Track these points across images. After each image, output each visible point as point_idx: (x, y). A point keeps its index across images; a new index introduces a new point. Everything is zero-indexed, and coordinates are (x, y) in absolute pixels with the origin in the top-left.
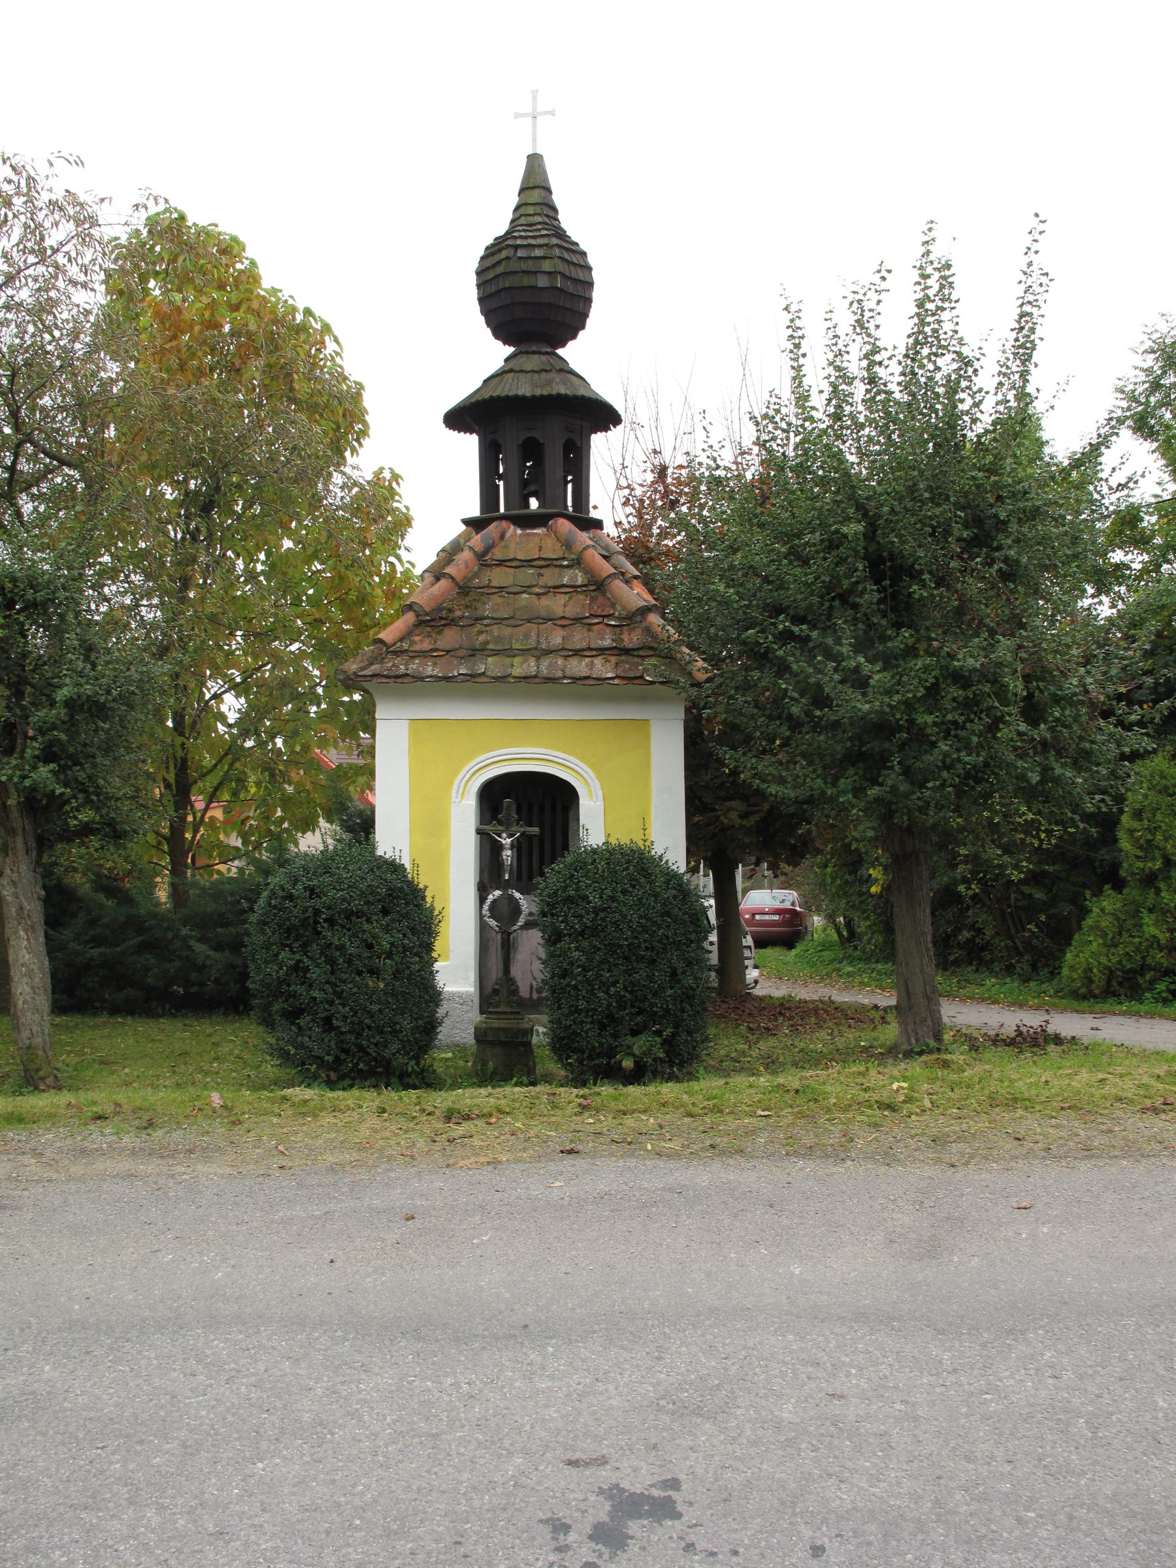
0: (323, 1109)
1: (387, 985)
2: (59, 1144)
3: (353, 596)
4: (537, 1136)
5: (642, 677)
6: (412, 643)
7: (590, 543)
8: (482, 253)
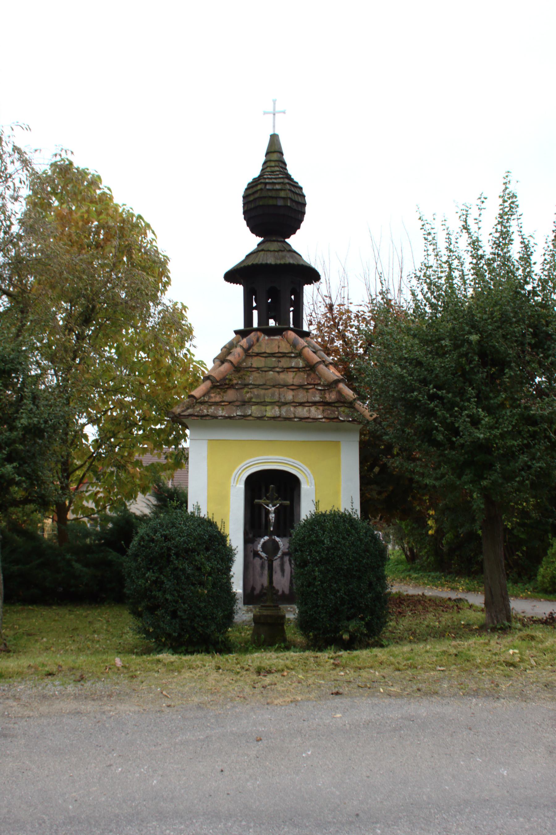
0: (183, 667)
1: (208, 591)
2: (29, 692)
3: (163, 371)
4: (314, 684)
5: (338, 418)
6: (210, 397)
7: (306, 344)
8: (246, 187)
